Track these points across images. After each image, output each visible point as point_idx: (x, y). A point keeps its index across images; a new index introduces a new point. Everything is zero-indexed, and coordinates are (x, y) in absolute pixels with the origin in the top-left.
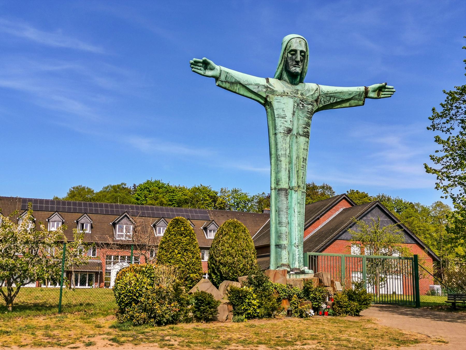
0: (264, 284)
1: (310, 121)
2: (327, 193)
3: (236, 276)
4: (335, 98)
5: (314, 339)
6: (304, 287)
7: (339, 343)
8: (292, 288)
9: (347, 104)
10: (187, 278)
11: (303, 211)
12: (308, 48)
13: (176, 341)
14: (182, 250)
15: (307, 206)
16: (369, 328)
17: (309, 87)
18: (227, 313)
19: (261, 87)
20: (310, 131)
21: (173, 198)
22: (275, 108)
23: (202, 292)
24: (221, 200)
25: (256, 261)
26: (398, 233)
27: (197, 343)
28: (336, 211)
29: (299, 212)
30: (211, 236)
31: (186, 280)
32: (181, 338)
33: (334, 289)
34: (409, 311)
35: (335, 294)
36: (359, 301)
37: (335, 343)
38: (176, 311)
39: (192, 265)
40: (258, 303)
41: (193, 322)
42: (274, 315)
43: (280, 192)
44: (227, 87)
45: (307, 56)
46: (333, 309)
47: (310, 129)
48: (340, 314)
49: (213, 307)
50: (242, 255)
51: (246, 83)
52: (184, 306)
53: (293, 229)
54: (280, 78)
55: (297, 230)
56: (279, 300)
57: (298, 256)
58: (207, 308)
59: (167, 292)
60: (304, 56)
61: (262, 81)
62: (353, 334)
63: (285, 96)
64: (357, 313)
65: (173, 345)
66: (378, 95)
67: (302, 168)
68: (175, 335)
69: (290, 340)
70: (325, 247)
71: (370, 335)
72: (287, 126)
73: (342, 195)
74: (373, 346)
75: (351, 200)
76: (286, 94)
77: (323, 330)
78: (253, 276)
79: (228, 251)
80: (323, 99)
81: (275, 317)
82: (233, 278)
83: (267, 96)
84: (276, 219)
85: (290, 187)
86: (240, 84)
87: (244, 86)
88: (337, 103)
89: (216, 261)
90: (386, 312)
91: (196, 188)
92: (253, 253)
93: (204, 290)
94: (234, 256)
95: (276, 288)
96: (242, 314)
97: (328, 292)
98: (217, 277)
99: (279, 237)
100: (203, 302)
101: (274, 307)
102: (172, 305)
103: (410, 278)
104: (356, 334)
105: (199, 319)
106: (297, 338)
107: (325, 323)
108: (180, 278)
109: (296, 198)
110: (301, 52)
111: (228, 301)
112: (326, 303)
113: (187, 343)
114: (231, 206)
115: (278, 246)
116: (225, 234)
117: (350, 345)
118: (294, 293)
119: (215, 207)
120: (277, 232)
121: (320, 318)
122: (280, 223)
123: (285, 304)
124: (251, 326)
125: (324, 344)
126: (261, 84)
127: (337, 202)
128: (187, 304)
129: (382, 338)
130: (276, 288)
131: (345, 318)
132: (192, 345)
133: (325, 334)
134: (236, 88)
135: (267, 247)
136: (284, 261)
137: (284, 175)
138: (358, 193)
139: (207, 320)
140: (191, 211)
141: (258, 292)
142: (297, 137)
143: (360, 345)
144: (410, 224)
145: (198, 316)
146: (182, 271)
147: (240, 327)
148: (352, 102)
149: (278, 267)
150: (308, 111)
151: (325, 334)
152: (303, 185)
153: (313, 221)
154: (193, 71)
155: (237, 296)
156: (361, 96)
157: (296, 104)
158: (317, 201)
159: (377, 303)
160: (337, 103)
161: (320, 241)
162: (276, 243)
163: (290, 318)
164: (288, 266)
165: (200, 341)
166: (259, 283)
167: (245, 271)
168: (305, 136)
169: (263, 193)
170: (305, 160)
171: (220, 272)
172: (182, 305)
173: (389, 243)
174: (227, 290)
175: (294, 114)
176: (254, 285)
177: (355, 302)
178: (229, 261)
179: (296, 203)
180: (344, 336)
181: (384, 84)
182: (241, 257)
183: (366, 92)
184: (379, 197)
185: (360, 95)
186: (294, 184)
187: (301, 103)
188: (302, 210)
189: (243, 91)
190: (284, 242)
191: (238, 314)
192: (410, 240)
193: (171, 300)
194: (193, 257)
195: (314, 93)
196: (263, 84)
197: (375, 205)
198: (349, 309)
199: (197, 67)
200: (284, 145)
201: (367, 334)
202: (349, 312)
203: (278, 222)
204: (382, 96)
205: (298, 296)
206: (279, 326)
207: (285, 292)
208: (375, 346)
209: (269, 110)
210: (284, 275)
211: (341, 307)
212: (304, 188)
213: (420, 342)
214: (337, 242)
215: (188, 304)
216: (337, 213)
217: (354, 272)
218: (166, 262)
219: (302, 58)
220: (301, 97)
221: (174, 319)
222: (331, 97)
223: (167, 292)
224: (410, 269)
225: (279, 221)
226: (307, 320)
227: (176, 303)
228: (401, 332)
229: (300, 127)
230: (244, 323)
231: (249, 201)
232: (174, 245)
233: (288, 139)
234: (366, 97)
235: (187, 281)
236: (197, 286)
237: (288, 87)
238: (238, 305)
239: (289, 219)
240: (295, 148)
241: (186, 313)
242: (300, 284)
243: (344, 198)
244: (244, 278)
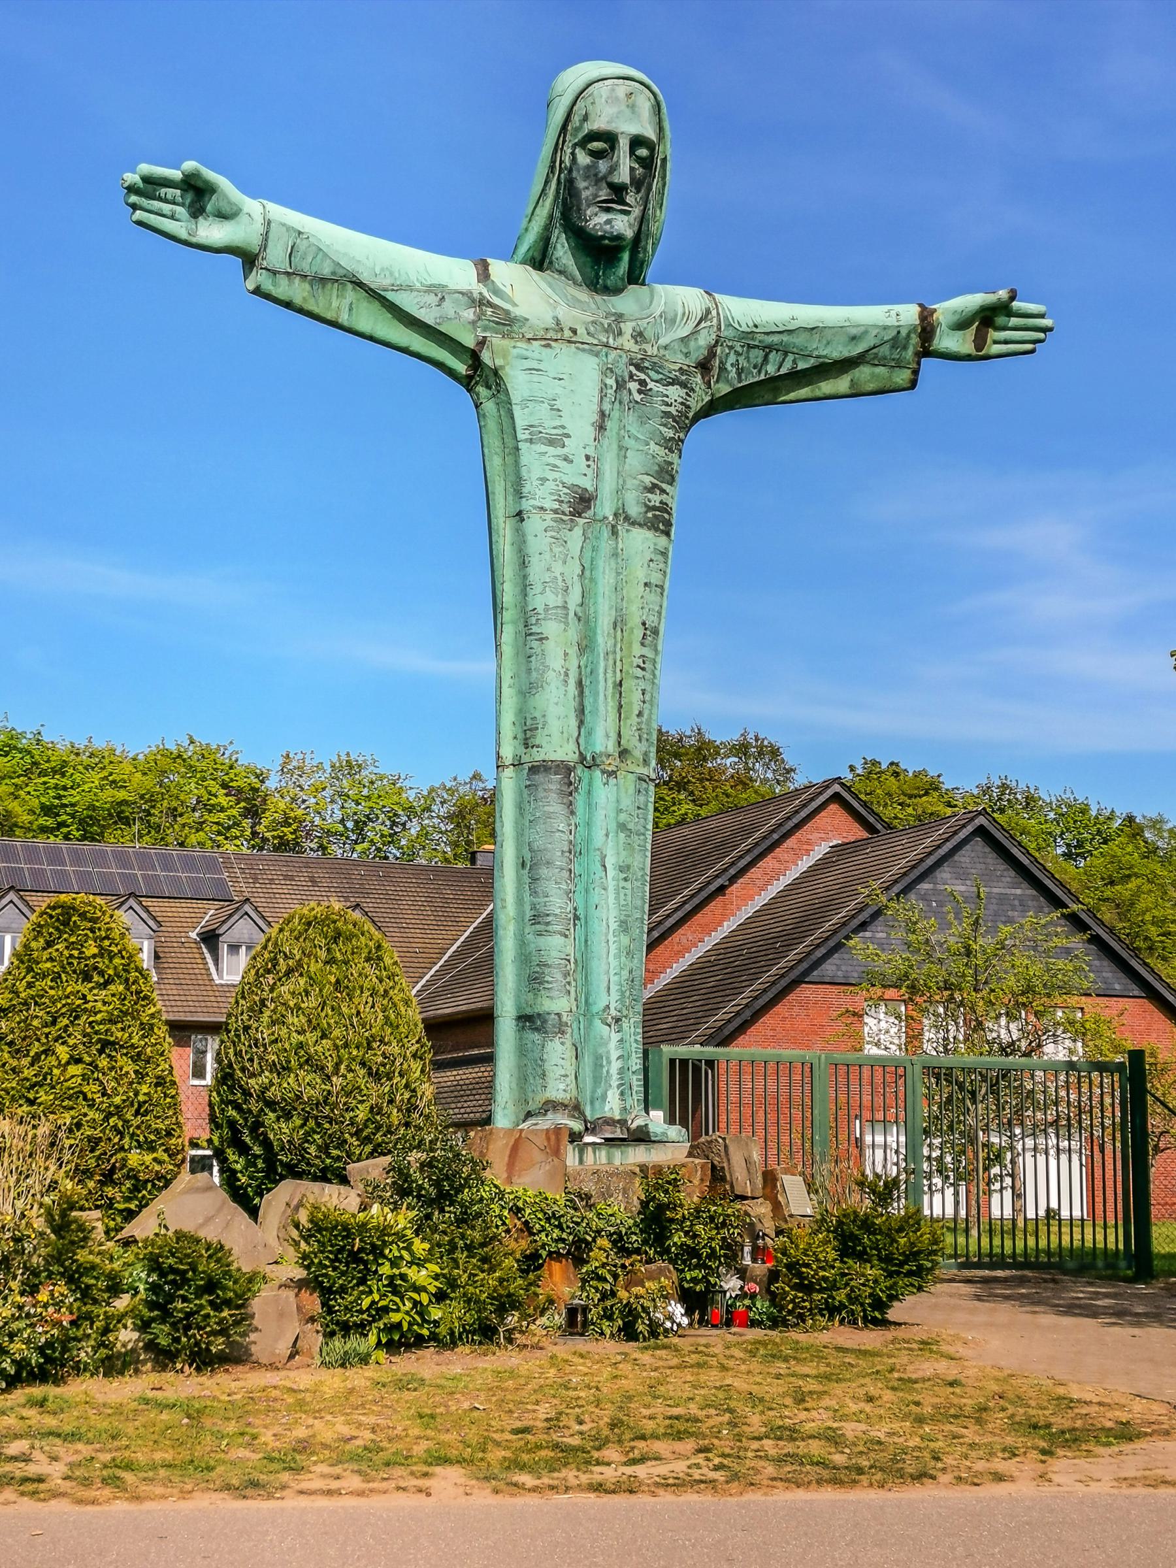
0: (466, 1195)
1: (674, 457)
2: (761, 771)
3: (339, 1159)
4: (786, 353)
5: (679, 1436)
6: (644, 1204)
7: (789, 1448)
8: (590, 1207)
9: (842, 384)
10: (113, 1170)
11: (642, 862)
12: (667, 125)
13: (55, 1459)
14: (88, 1045)
15: (661, 835)
16: (924, 1380)
17: (672, 305)
18: (293, 1327)
19: (456, 301)
20: (674, 505)
21: (59, 797)
22: (515, 397)
23: (180, 1236)
24: (282, 806)
25: (427, 1090)
26: (1068, 951)
27: (154, 1468)
28: (798, 855)
29: (624, 869)
30: (232, 970)
31: (108, 1178)
32: (80, 1446)
33: (777, 1207)
34: (1102, 1294)
35: (779, 1232)
36: (888, 1259)
37: (772, 1452)
38: (57, 1324)
39: (137, 1113)
40: (436, 1277)
41: (137, 1371)
42: (510, 1331)
43: (539, 778)
44: (298, 301)
45: (664, 160)
46: (773, 1297)
47: (674, 496)
48: (802, 1318)
49: (228, 1303)
50: (363, 1064)
51: (386, 282)
52: (95, 1302)
53: (598, 947)
54: (540, 260)
55: (613, 947)
56: (531, 1262)
57: (619, 1064)
58: (201, 1307)
59: (17, 1240)
60: (647, 164)
61: (458, 273)
62: (854, 1407)
63: (564, 346)
64: (875, 1313)
65: (40, 1480)
66: (980, 342)
67: (639, 673)
68: (51, 1434)
69: (575, 1441)
70: (747, 1014)
71: (927, 1410)
72: (570, 480)
73: (827, 785)
74: (937, 1459)
75: (865, 805)
76: (567, 334)
77: (721, 1395)
78: (415, 1157)
79: (301, 1045)
80: (732, 359)
81: (510, 1341)
82: (324, 1170)
83: (482, 343)
84: (520, 901)
85: (582, 758)
86: (359, 284)
87: (375, 295)
88: (798, 378)
89: (247, 1093)
90: (1006, 1306)
91: (166, 753)
92: (414, 1056)
93: (188, 1227)
94: (330, 1069)
95: (517, 1211)
96: (362, 1328)
97: (752, 1224)
98: (251, 1163)
99: (534, 978)
100: (185, 1281)
101: (509, 1295)
102: (43, 1296)
103: (1113, 1148)
104: (868, 1408)
105: (164, 1358)
106: (606, 1432)
107: (731, 1363)
108: (81, 1174)
109: (612, 805)
110: (637, 142)
111: (300, 1273)
112: (742, 1273)
113: (105, 1466)
114: (328, 833)
115: (528, 1020)
116: (289, 972)
117: (839, 1459)
118: (598, 1232)
119: (258, 842)
120: (524, 957)
121: (711, 1340)
122: (538, 918)
123: (557, 1277)
124: (402, 1384)
125: (724, 1456)
126: (452, 286)
127: (803, 814)
128: (109, 1289)
129: (979, 1421)
130: (517, 1211)
131: (824, 1337)
132: (128, 1477)
133: (731, 1411)
134: (342, 304)
135: (484, 1019)
136: (558, 1090)
137: (555, 703)
138: (896, 774)
139: (204, 1361)
140: (144, 860)
141: (435, 1230)
142: (614, 532)
143: (884, 1457)
144: (1124, 908)
145: (163, 1341)
146: (90, 1139)
147: (352, 1391)
148: (864, 374)
149: (529, 1115)
150: (667, 414)
151: (731, 1411)
152: (643, 747)
153: (696, 901)
154: (140, 223)
155: (343, 1248)
156: (905, 348)
157: (611, 382)
158: (710, 812)
159: (967, 1265)
160: (798, 378)
161: (728, 990)
162: (519, 1008)
163: (579, 1344)
164: (576, 1109)
165: (168, 1456)
166: (442, 1192)
167: (379, 1137)
168: (652, 525)
169: (476, 777)
170: (651, 632)
171: (266, 1144)
172: (86, 1294)
173: (1024, 1000)
174: (297, 1226)
175: (601, 428)
176: (419, 1197)
177: (873, 1261)
178: (308, 1093)
179: (613, 826)
180: (815, 1419)
181: (1003, 294)
182: (362, 1072)
183: (927, 329)
184: (986, 791)
185: (897, 342)
186: (602, 742)
187: (633, 377)
188: (638, 857)
189: (370, 319)
190: (557, 1003)
191: (346, 1329)
192: (1119, 982)
193: (35, 1273)
194: (141, 1076)
195: (695, 332)
196: (464, 287)
197: (970, 829)
198: (841, 1296)
199: (156, 205)
200: (558, 568)
201: (917, 1404)
202: (842, 1306)
203: (529, 914)
204: (996, 349)
205: (614, 1243)
206: (529, 1378)
207: (560, 1227)
208: (949, 1461)
209: (489, 406)
210: (557, 1152)
211: (808, 1289)
212: (646, 762)
213: (1140, 1436)
214: (806, 992)
215: (115, 1289)
216: (804, 864)
217: (879, 1127)
218: (13, 1099)
219: (640, 171)
220: (635, 348)
221: (49, 1360)
222: (768, 349)
223: (17, 1240)
224: (1113, 1112)
225: (533, 907)
226: (657, 1347)
227: (61, 1288)
228: (1061, 1391)
229: (631, 483)
230: (370, 1372)
231: (410, 810)
232: (54, 1023)
233: (575, 537)
234: (926, 352)
235: (114, 1183)
236: (157, 1205)
237: (574, 303)
238: (343, 1290)
239: (579, 900)
240: (605, 579)
241: (106, 1331)
242: (625, 1191)
243: (836, 797)
244: (375, 1168)
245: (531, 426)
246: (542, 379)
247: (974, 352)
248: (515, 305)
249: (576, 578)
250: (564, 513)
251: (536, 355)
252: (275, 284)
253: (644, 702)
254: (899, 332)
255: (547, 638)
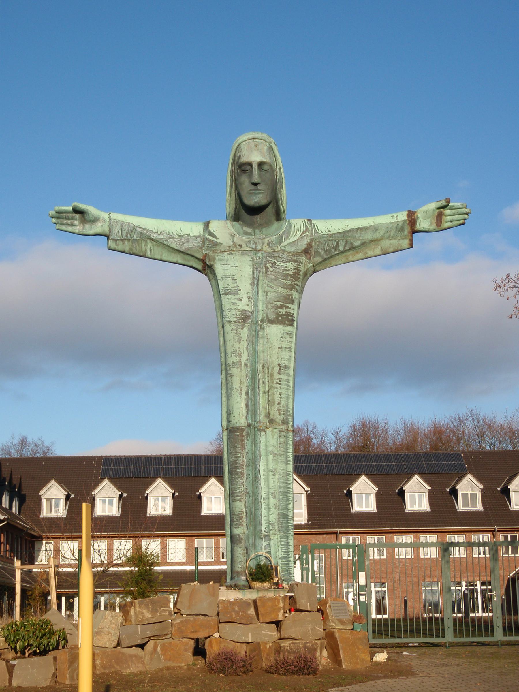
22: (219, 276)
61: (195, 229)
67: (278, 386)
110: (261, 164)
183: (412, 220)
189: (159, 252)
204: (447, 225)
234: (414, 232)
245: (225, 288)
246: (228, 268)
247: (437, 229)
248: (217, 238)
249: (245, 349)
250: (239, 322)
251: (226, 258)
252: (117, 245)
253: (281, 398)
254: (398, 224)
255: (233, 376)
